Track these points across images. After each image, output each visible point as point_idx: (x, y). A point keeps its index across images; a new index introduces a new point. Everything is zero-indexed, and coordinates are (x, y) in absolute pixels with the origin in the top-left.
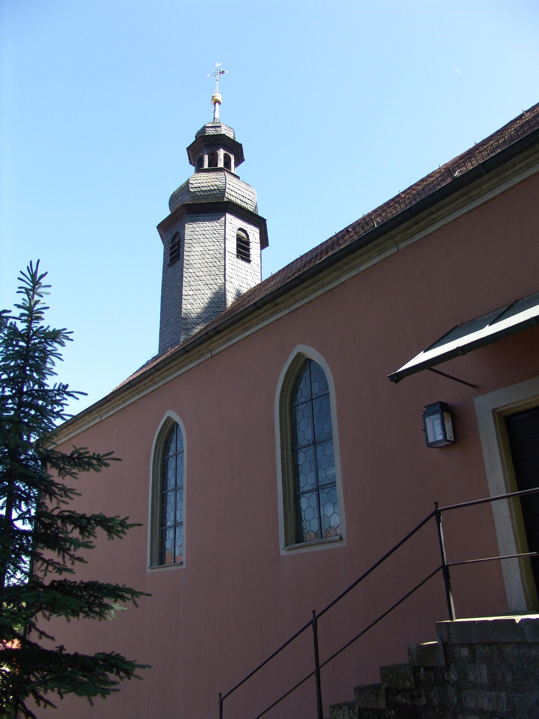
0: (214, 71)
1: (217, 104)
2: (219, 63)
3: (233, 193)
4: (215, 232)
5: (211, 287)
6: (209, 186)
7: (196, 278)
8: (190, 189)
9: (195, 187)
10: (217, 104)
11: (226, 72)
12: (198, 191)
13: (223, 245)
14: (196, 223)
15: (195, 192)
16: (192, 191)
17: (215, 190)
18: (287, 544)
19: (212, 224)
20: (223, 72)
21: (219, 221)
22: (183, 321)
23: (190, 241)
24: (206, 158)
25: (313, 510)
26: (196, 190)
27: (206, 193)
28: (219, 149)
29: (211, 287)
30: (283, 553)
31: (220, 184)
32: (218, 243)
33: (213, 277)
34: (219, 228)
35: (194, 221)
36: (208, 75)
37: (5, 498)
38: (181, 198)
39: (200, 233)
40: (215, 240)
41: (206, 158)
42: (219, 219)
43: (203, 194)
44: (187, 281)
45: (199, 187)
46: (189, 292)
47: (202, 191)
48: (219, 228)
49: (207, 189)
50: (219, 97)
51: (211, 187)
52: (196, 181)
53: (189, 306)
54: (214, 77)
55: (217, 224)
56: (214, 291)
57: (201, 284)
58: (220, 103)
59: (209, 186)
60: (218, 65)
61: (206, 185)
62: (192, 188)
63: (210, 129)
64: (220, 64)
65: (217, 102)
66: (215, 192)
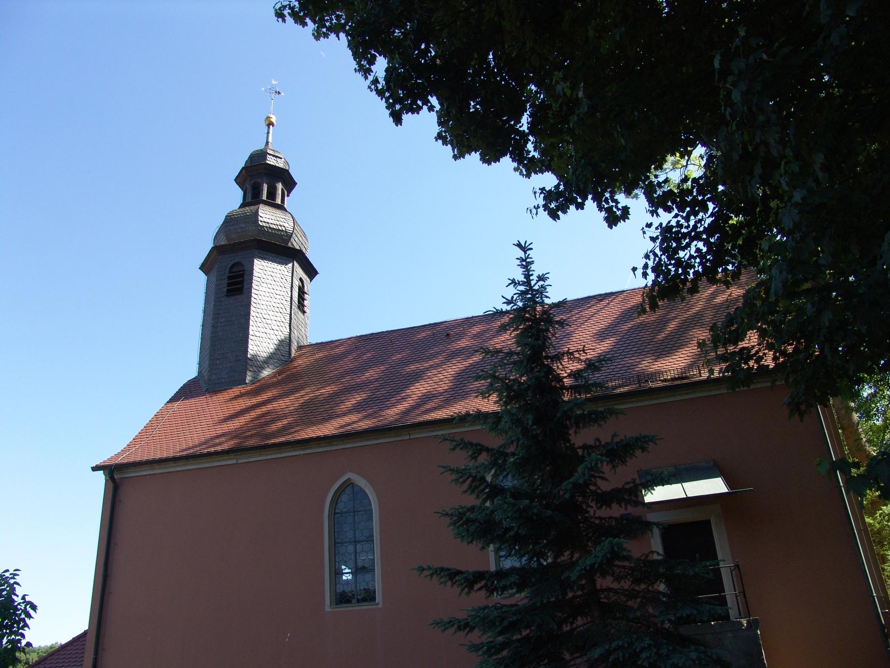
0: (269, 87)
1: (271, 126)
2: (275, 81)
3: (296, 239)
4: (282, 276)
5: (277, 333)
6: (277, 225)
7: (263, 320)
8: (259, 222)
9: (264, 222)
10: (271, 126)
11: (282, 94)
12: (266, 227)
13: (289, 293)
14: (265, 261)
15: (264, 226)
16: (261, 224)
17: (283, 231)
18: (331, 605)
19: (281, 268)
20: (279, 93)
21: (286, 266)
22: (250, 363)
23: (258, 279)
24: (265, 187)
25: (362, 550)
26: (264, 224)
27: (273, 231)
28: (278, 182)
29: (277, 333)
30: (328, 609)
31: (288, 226)
32: (284, 289)
33: (278, 323)
34: (287, 273)
35: (263, 258)
36: (263, 89)
37: (719, 191)
38: (244, 226)
39: (269, 273)
40: (282, 286)
41: (265, 187)
42: (286, 264)
43: (270, 231)
44: (254, 320)
45: (268, 223)
46: (255, 333)
47: (270, 228)
48: (287, 273)
49: (275, 228)
50: (273, 120)
51: (279, 226)
52: (266, 216)
53: (256, 349)
54: (268, 93)
55: (285, 269)
56: (279, 339)
57: (267, 327)
58: (273, 124)
59: (277, 225)
60: (274, 82)
61: (275, 223)
62: (261, 221)
63: (271, 157)
64: (276, 82)
65: (270, 124)
66: (282, 233)
